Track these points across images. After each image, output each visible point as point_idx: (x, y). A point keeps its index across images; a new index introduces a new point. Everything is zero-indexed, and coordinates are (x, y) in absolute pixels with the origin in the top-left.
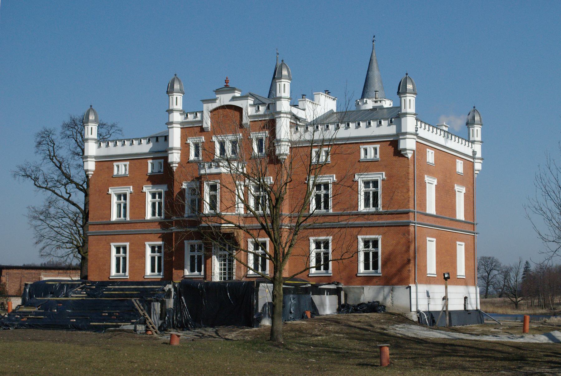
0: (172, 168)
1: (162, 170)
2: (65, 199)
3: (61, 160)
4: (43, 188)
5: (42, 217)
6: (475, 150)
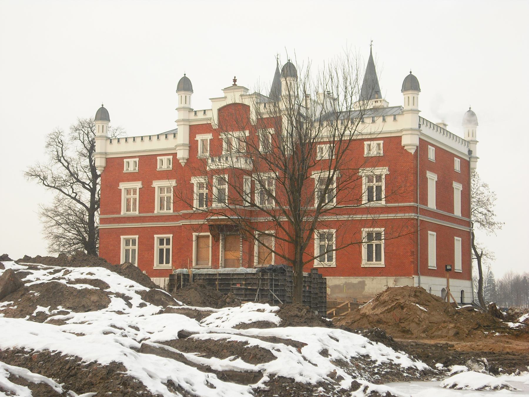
0: (180, 163)
2: (72, 198)
3: (69, 160)
4: (51, 187)
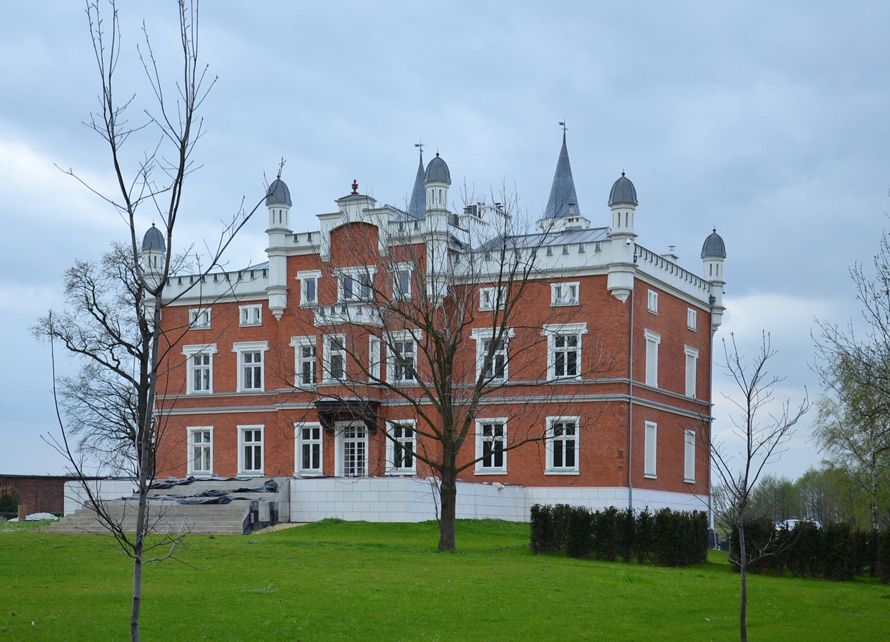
1: (260, 320)
2: (112, 368)
5: (81, 395)
6: (713, 296)
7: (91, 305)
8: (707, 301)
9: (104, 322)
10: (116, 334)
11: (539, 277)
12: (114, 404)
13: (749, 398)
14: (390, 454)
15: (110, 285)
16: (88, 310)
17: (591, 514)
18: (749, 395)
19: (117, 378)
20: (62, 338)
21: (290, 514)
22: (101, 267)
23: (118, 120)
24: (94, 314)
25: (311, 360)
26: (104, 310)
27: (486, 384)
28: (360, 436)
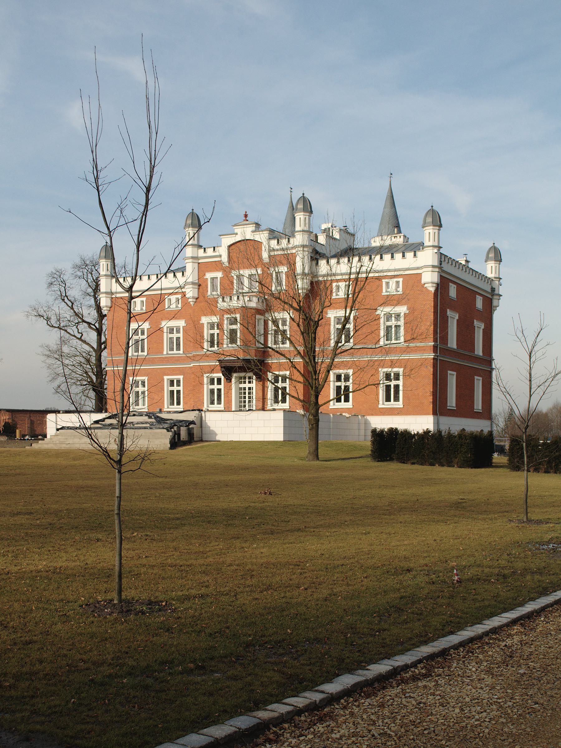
2: (78, 338)
7: (64, 298)
8: (489, 290)
9: (72, 308)
10: (80, 316)
11: (377, 275)
12: (79, 362)
13: (530, 356)
14: (270, 394)
15: (76, 283)
16: (61, 300)
17: (413, 434)
18: (530, 354)
19: (81, 345)
20: (44, 319)
21: (202, 435)
22: (70, 271)
23: (101, 175)
24: (65, 302)
25: (216, 331)
26: (72, 299)
27: (340, 347)
28: (250, 382)
